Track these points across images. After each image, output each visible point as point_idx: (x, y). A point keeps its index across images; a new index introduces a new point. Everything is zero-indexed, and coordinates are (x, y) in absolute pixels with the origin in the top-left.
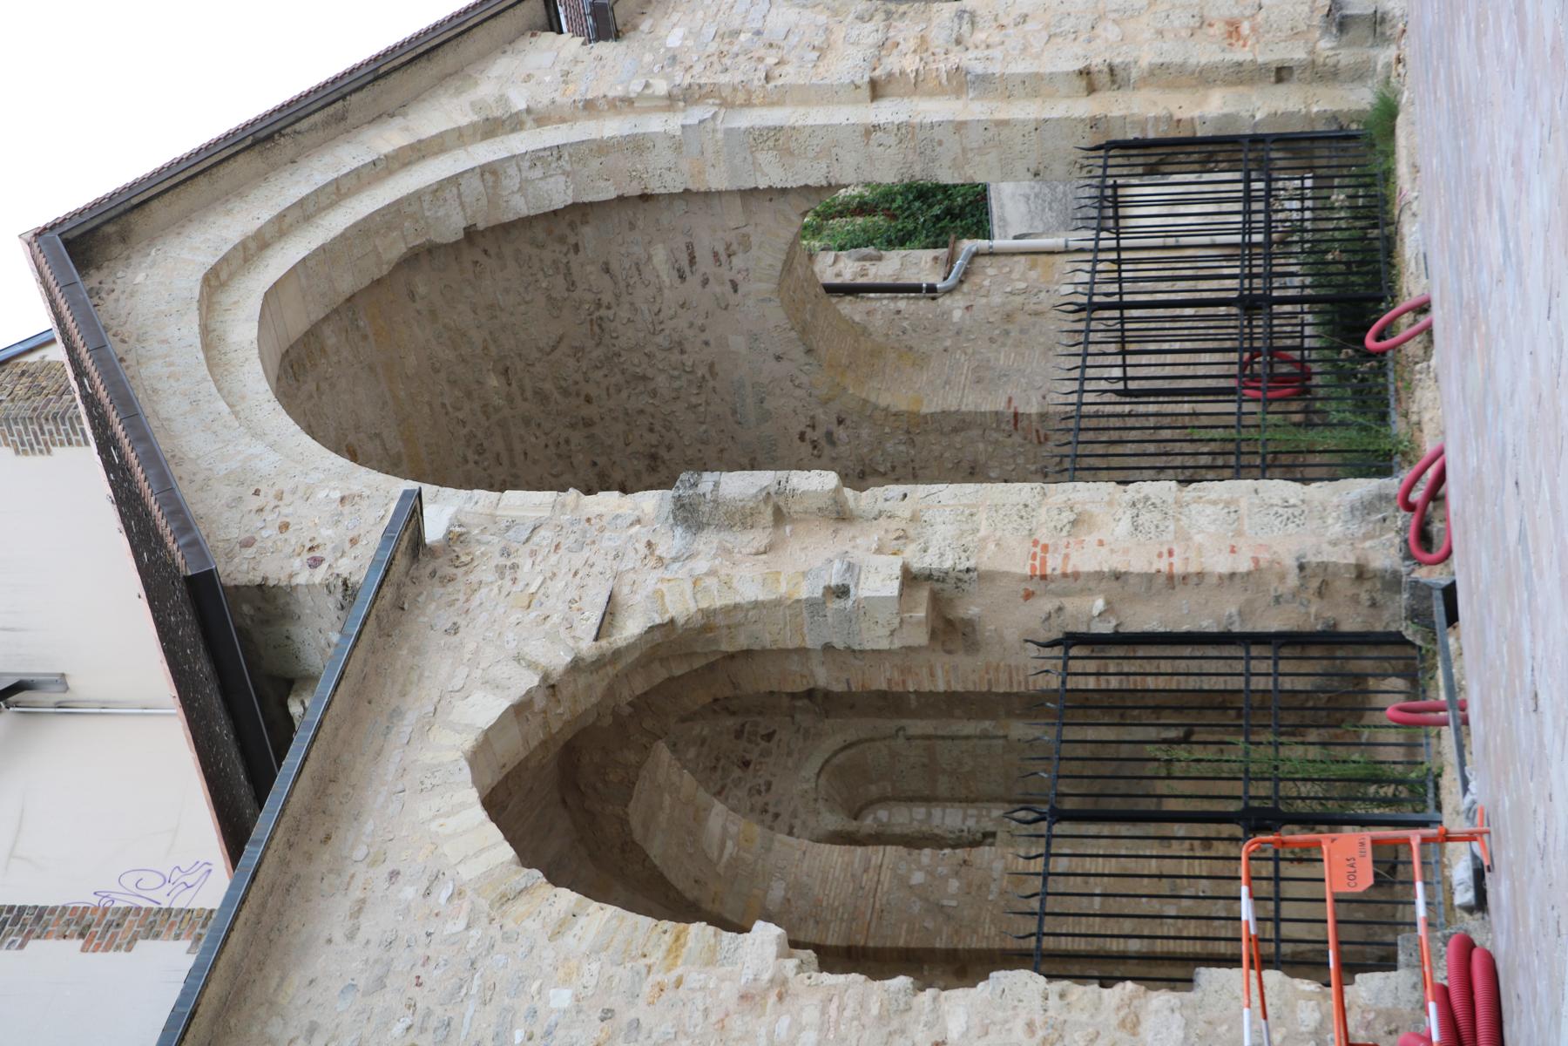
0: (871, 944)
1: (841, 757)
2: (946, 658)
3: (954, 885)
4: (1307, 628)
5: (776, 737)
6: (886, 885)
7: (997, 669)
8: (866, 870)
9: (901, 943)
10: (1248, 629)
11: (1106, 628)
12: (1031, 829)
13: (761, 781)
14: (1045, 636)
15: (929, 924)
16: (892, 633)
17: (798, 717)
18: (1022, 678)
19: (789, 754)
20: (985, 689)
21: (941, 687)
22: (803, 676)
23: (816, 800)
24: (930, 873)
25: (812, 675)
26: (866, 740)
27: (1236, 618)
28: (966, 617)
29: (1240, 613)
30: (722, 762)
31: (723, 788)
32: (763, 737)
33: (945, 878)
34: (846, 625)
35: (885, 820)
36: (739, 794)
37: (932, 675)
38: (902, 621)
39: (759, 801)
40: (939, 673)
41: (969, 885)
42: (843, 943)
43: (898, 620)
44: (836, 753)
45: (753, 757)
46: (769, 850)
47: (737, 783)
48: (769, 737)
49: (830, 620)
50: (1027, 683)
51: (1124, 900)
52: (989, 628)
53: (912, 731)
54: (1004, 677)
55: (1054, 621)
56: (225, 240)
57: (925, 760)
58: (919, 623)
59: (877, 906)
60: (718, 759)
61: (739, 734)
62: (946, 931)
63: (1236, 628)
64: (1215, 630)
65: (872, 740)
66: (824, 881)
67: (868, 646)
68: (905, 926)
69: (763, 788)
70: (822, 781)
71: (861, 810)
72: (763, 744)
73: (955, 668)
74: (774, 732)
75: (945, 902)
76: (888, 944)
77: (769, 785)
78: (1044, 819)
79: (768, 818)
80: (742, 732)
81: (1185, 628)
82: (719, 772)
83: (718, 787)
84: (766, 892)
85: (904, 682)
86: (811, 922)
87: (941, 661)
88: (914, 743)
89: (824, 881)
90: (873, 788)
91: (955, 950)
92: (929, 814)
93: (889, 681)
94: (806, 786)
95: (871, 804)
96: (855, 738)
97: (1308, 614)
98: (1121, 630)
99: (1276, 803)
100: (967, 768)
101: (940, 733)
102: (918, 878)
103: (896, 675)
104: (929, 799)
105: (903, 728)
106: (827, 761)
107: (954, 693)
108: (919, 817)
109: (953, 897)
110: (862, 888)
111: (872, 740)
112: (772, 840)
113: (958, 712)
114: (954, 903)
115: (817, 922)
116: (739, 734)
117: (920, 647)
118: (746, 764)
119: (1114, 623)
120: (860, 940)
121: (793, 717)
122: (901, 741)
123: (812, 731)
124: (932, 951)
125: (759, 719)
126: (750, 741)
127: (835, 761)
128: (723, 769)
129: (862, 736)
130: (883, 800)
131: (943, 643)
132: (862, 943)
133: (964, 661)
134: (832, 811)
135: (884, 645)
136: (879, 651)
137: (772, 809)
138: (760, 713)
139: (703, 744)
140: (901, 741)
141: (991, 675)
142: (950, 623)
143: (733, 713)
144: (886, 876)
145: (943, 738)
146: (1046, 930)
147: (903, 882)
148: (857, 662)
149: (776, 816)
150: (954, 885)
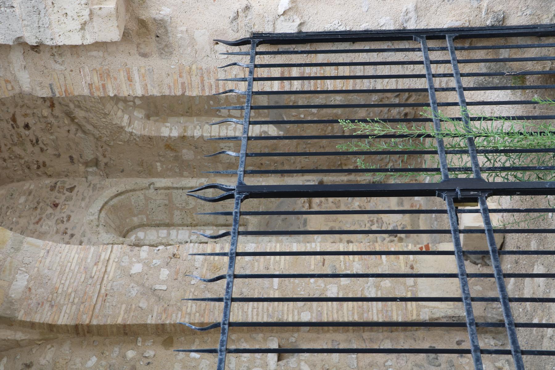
0: (95, 322)
1: (115, 201)
2: (142, 61)
3: (165, 273)
4: (477, 24)
5: (76, 190)
7: (190, 72)
9: (120, 321)
10: (422, 26)
11: (288, 27)
12: (220, 206)
13: (64, 215)
14: (234, 37)
15: (143, 304)
16: (84, 26)
17: (90, 178)
18: (213, 81)
19: (83, 199)
20: (179, 93)
21: (139, 92)
22: (7, 81)
23: (98, 226)
24: (147, 264)
25: (16, 80)
26: (131, 191)
27: (412, 14)
28: (159, 17)
29: (416, 9)
30: (41, 204)
31: (40, 219)
32: (67, 190)
33: (159, 268)
34: (35, 18)
35: (142, 238)
36: (50, 223)
37: (130, 79)
38: (91, 14)
39: (62, 227)
40: (136, 77)
41: (177, 273)
42: (73, 323)
43: (86, 13)
44: (112, 198)
45: (60, 201)
46: (18, 250)
47: (49, 217)
48: (71, 189)
49: (17, 11)
50: (217, 86)
51: (297, 280)
52: (179, 31)
53: (158, 185)
54: (196, 80)
55: (242, 21)
56: (244, 283)
57: (167, 202)
58: (109, 16)
59: (103, 291)
60: (38, 203)
61: (53, 188)
62: (157, 309)
63: (411, 26)
64: (392, 28)
65: (134, 190)
66: (62, 273)
67: (61, 41)
68: (124, 306)
69: (65, 219)
70: (103, 214)
71: (128, 232)
72: (68, 193)
73: (151, 71)
74: (75, 186)
75: (157, 287)
76: (109, 322)
77: (69, 217)
78: (231, 196)
79: (67, 237)
80: (55, 187)
81: (363, 27)
82: (38, 211)
83: (37, 219)
84: (10, 284)
85: (104, 86)
86: (47, 306)
87: (137, 64)
88: (159, 192)
89: (62, 273)
90: (135, 219)
91: (163, 325)
92: (169, 234)
93: (90, 85)
94: (92, 218)
95: (134, 228)
96: (124, 189)
97: (479, 8)
98: (304, 30)
99: (478, 174)
100: (191, 206)
101: (175, 186)
102: (137, 268)
103: (96, 79)
104: (168, 225)
105: (153, 183)
106: (106, 203)
107: (152, 97)
108: (163, 236)
109: (164, 282)
110: (92, 278)
111: (134, 190)
112: (22, 242)
113: (185, 173)
114: (164, 287)
115: (52, 306)
116: (53, 188)
117: (113, 43)
118: (56, 205)
119: (298, 22)
120: (85, 320)
121: (87, 178)
122: (152, 190)
123: (98, 186)
124: (145, 326)
125: (66, 179)
126: (59, 192)
127: (112, 203)
128: (41, 209)
129: (128, 188)
130: (142, 226)
131: (138, 46)
132: (87, 322)
133: (156, 63)
134: (107, 232)
135: (76, 40)
136: (76, 46)
137: (69, 232)
138: (67, 176)
139: (30, 194)
140: (152, 190)
141: (185, 79)
142: (142, 23)
143: (50, 176)
144: (112, 268)
145: (177, 188)
146: (240, 250)
147: (125, 272)
148: (57, 67)
149: (72, 236)
150: (165, 273)
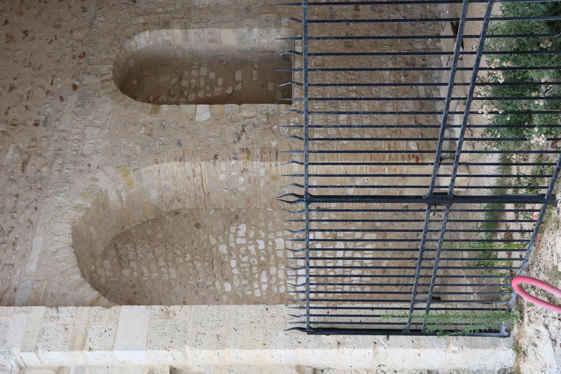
3: (242, 180)
6: (207, 181)
8: (194, 176)
